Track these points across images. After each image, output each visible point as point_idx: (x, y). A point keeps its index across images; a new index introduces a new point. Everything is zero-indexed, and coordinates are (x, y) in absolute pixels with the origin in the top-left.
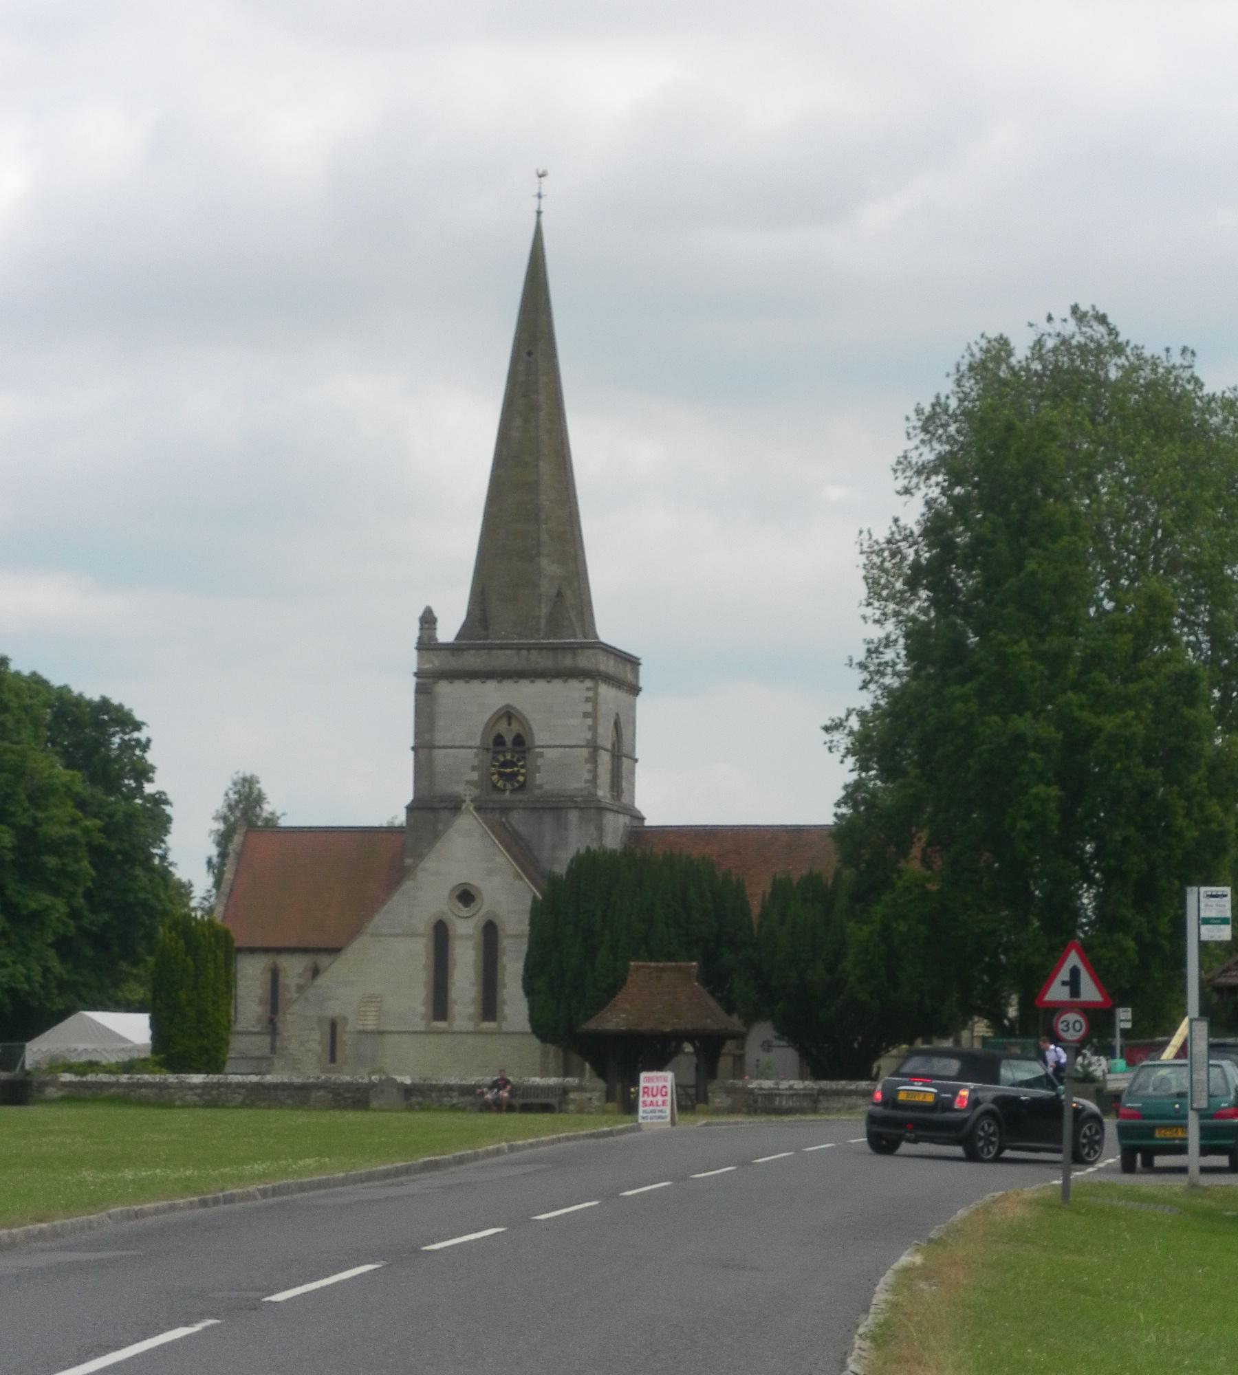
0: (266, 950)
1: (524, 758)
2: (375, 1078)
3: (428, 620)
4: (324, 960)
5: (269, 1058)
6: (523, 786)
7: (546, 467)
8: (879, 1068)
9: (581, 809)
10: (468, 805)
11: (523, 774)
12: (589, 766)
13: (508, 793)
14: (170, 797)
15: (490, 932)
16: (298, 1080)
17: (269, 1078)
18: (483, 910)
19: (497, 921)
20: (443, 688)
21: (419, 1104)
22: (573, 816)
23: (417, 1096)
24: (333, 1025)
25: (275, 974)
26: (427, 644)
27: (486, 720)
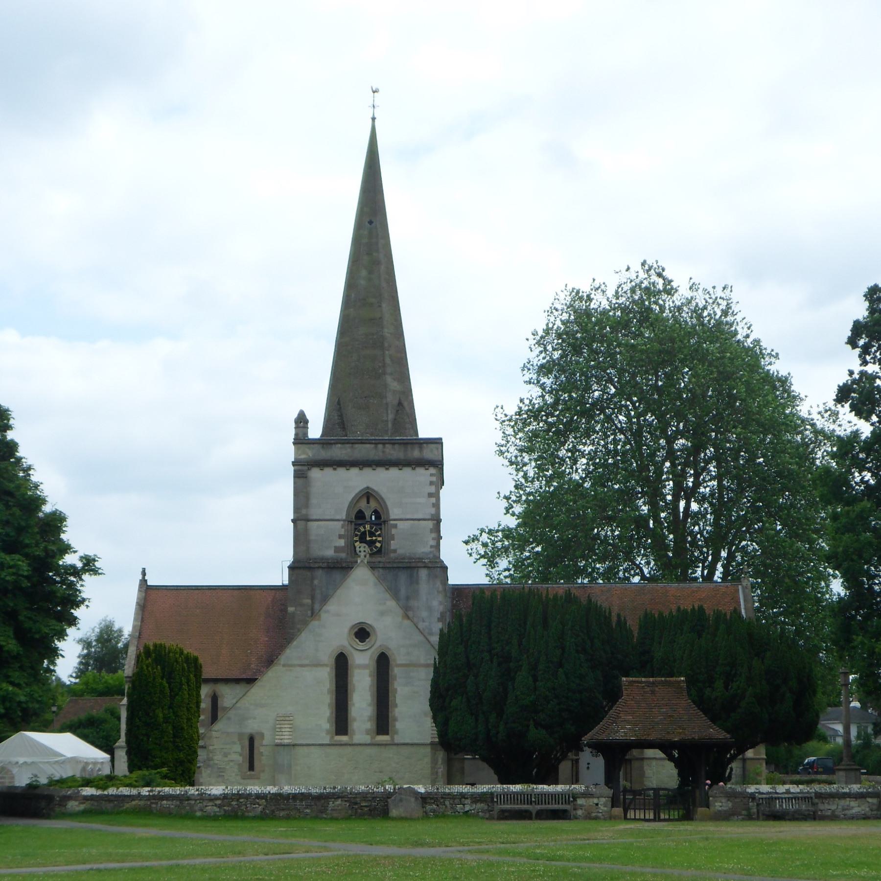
1: (381, 529)
2: (389, 787)
3: (302, 421)
6: (380, 551)
8: (731, 769)
9: (428, 567)
11: (379, 542)
12: (434, 535)
15: (383, 663)
16: (315, 791)
18: (378, 644)
20: (315, 474)
21: (434, 811)
22: (423, 573)
24: (252, 740)
26: (301, 440)
27: (350, 499)
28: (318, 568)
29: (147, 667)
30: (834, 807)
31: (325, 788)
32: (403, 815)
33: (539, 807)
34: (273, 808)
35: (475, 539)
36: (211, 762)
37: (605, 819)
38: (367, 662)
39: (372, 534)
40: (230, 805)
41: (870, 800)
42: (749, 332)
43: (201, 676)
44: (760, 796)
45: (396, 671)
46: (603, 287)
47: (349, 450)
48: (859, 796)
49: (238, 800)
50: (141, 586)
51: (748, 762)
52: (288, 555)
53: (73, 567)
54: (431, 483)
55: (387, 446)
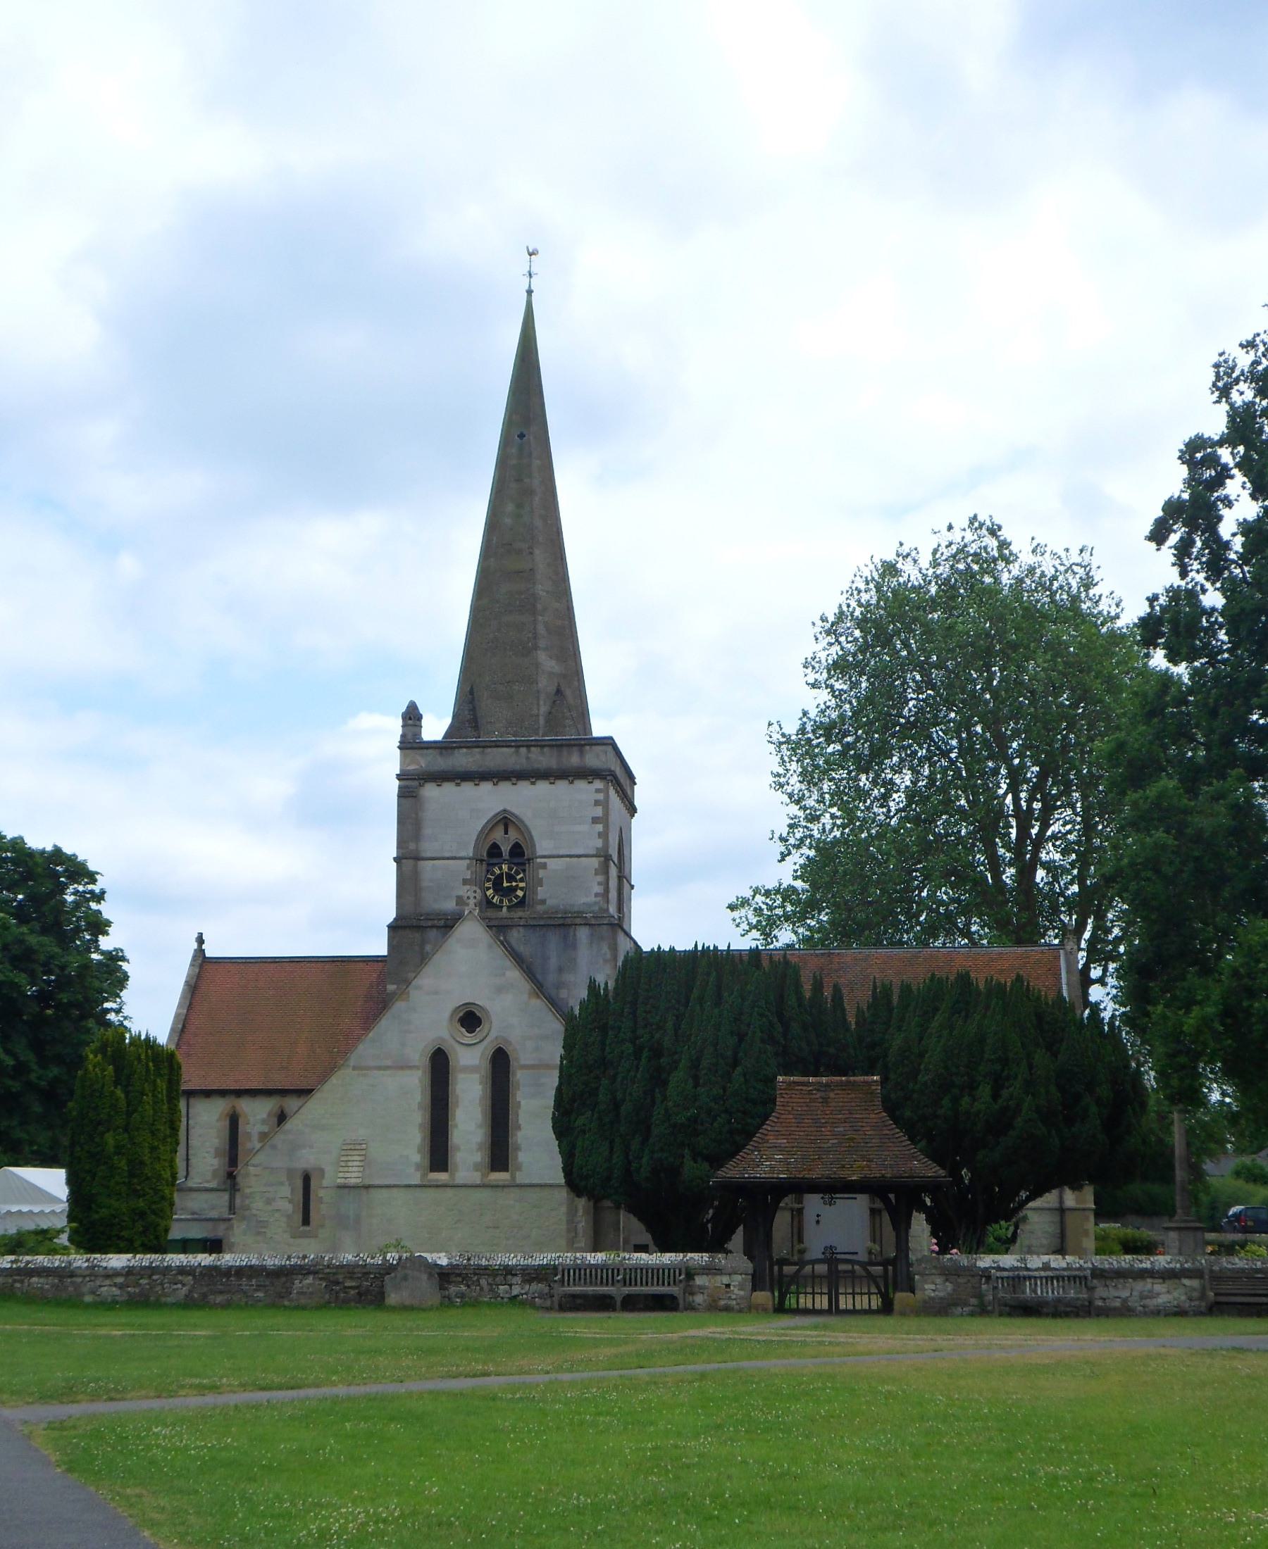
0: (222, 1093)
1: (524, 871)
2: (392, 1257)
3: (412, 717)
4: (291, 1103)
5: (229, 1220)
6: (522, 903)
7: (540, 558)
11: (522, 889)
12: (600, 878)
13: (505, 909)
14: (127, 954)
16: (271, 1262)
18: (493, 1034)
19: (509, 1050)
20: (431, 792)
21: (462, 1296)
22: (583, 934)
23: (459, 1285)
24: (307, 1179)
25: (234, 1121)
26: (410, 742)
28: (432, 927)
29: (95, 1067)
30: (1125, 1294)
31: (289, 1258)
32: (407, 1303)
33: (627, 1290)
34: (205, 1289)
35: (744, 902)
36: (247, 1213)
37: (740, 1311)
38: (476, 1062)
39: (511, 878)
40: (138, 1285)
41: (1186, 1282)
42: (1118, 610)
43: (178, 1082)
44: (999, 1274)
45: (520, 1076)
46: (914, 553)
47: (478, 756)
48: (1168, 1275)
49: (150, 1277)
50: (194, 958)
51: (1067, 1213)
52: (382, 901)
54: (597, 803)
55: (533, 749)
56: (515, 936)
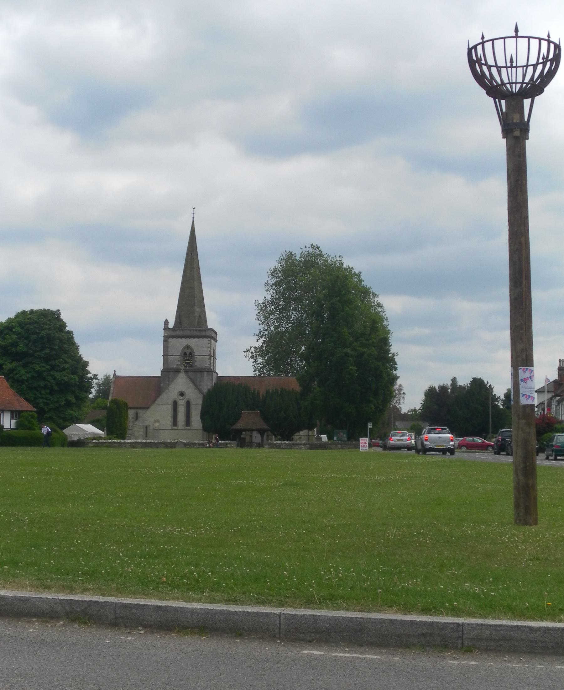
3: (166, 322)
4: (141, 412)
6: (191, 366)
10: (182, 371)
16: (156, 441)
17: (148, 441)
20: (170, 340)
22: (205, 373)
24: (147, 427)
26: (166, 329)
35: (248, 351)
45: (192, 407)
52: (160, 366)
53: (91, 377)
56: (190, 374)
